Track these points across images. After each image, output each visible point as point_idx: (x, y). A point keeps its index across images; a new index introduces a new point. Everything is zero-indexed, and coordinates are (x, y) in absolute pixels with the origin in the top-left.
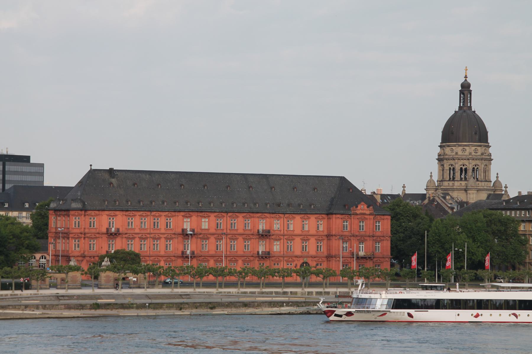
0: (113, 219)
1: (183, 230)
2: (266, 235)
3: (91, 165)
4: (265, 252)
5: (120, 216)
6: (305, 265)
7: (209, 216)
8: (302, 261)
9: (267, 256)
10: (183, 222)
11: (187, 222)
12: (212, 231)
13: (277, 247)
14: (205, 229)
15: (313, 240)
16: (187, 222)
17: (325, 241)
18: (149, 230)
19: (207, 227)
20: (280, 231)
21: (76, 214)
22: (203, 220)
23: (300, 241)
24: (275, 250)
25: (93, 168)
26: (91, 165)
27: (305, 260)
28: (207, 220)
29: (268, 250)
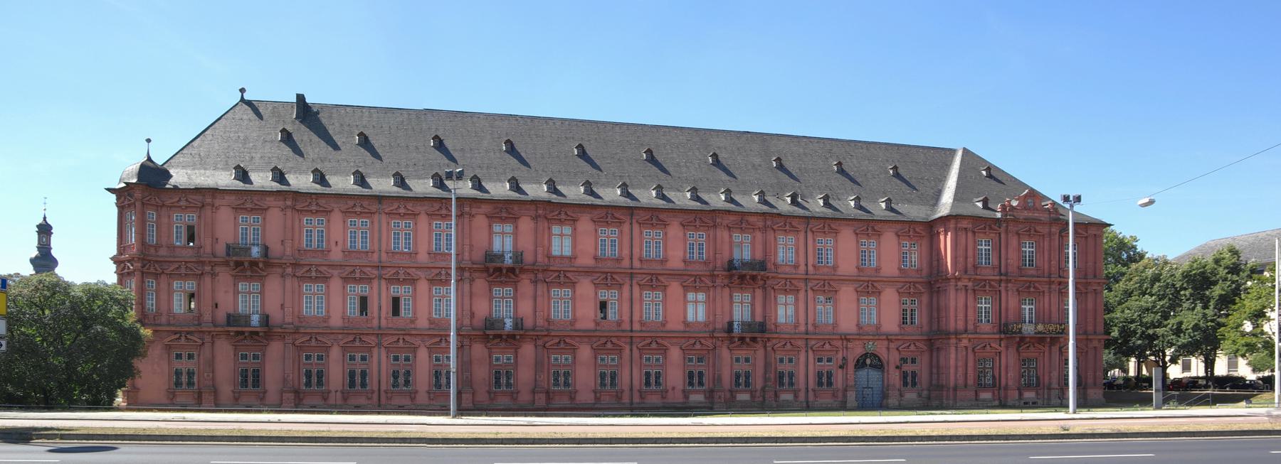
0: (913, 302)
1: (490, 257)
2: (754, 278)
3: (242, 91)
4: (749, 325)
5: (277, 210)
6: (868, 361)
7: (575, 221)
8: (859, 351)
9: (758, 333)
10: (686, 302)
11: (503, 233)
12: (586, 261)
13: (785, 311)
14: (562, 257)
15: (890, 295)
16: (503, 233)
17: (925, 299)
18: (376, 256)
19: (567, 252)
20: (619, 260)
21: (275, 217)
22: (556, 229)
23: (895, 297)
24: (781, 320)
25: (247, 97)
26: (242, 91)
27: (870, 347)
28: (567, 230)
29: (759, 319)
